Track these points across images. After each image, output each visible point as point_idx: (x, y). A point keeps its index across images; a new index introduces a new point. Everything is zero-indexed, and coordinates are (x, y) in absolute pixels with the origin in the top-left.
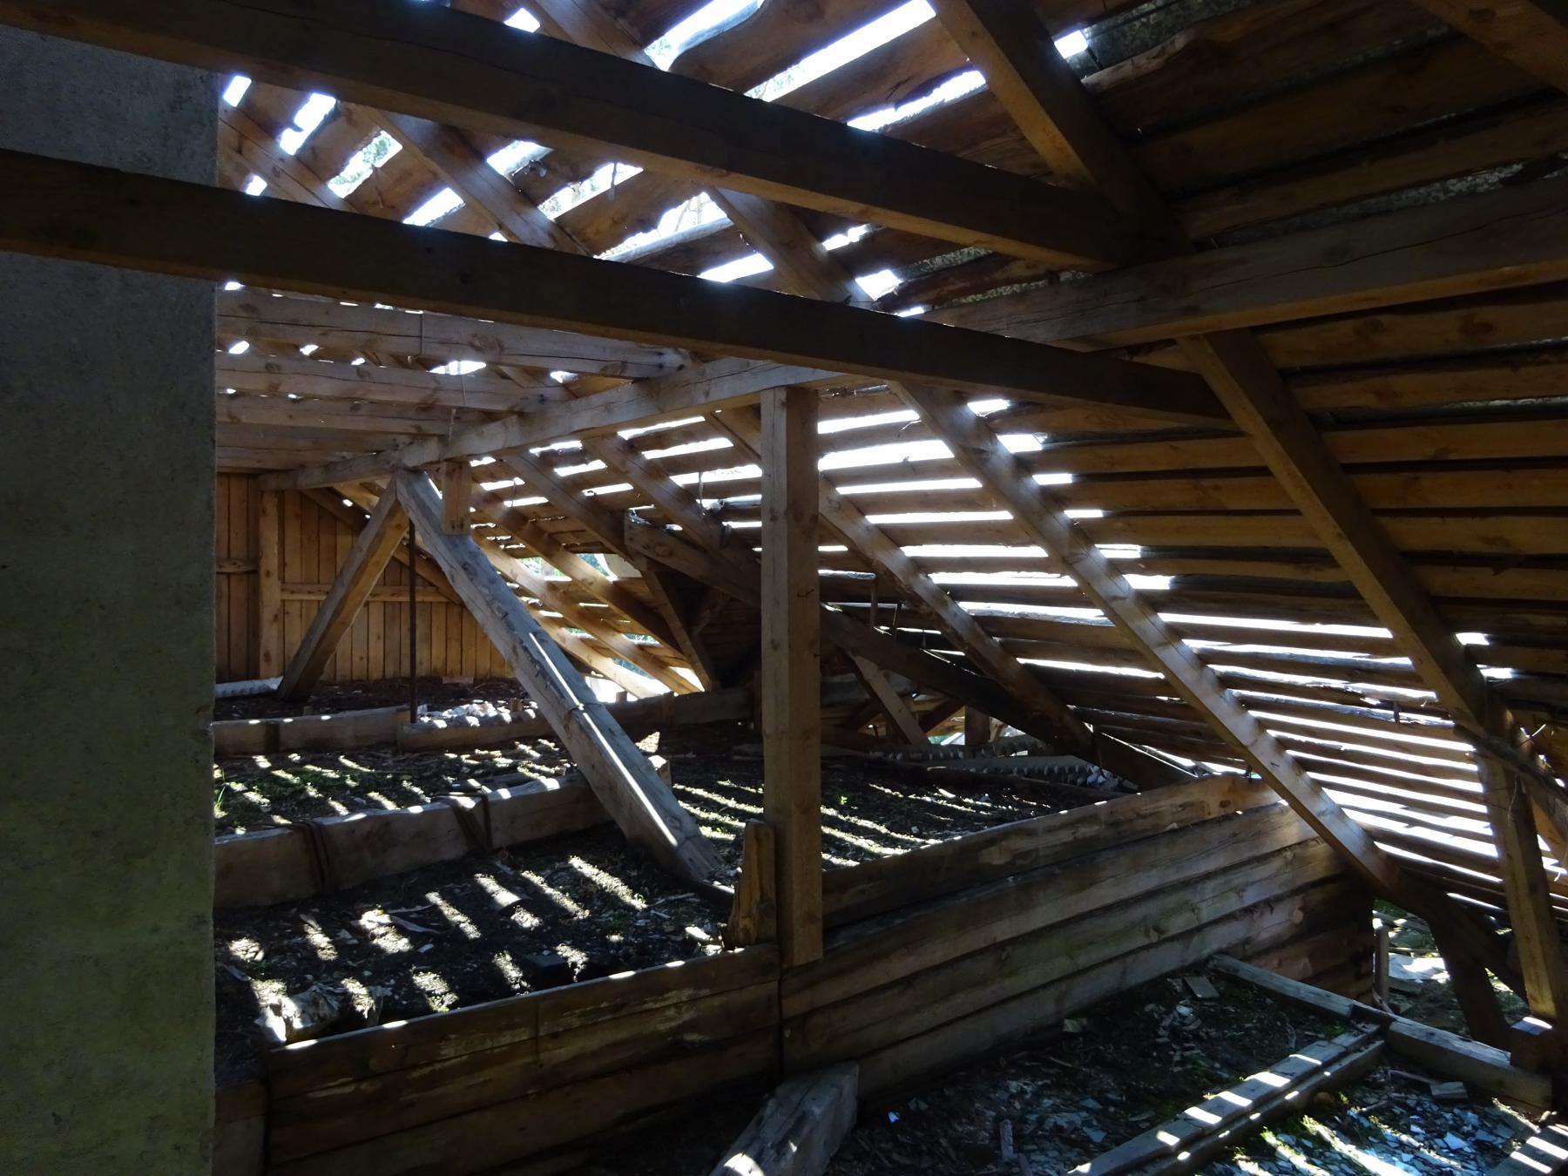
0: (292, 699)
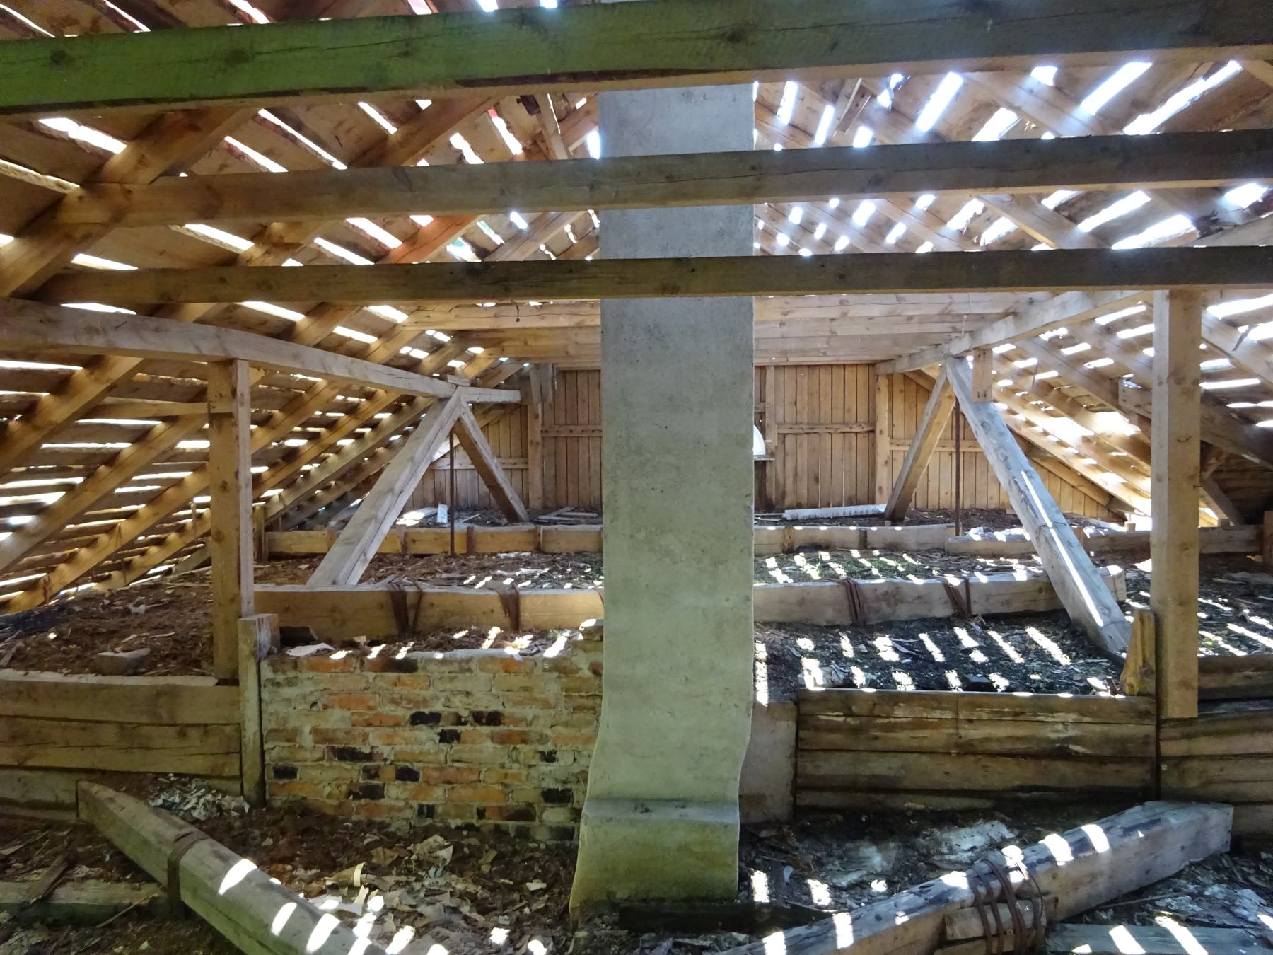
0: (895, 517)
